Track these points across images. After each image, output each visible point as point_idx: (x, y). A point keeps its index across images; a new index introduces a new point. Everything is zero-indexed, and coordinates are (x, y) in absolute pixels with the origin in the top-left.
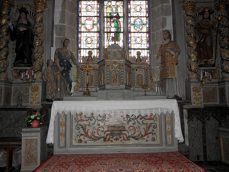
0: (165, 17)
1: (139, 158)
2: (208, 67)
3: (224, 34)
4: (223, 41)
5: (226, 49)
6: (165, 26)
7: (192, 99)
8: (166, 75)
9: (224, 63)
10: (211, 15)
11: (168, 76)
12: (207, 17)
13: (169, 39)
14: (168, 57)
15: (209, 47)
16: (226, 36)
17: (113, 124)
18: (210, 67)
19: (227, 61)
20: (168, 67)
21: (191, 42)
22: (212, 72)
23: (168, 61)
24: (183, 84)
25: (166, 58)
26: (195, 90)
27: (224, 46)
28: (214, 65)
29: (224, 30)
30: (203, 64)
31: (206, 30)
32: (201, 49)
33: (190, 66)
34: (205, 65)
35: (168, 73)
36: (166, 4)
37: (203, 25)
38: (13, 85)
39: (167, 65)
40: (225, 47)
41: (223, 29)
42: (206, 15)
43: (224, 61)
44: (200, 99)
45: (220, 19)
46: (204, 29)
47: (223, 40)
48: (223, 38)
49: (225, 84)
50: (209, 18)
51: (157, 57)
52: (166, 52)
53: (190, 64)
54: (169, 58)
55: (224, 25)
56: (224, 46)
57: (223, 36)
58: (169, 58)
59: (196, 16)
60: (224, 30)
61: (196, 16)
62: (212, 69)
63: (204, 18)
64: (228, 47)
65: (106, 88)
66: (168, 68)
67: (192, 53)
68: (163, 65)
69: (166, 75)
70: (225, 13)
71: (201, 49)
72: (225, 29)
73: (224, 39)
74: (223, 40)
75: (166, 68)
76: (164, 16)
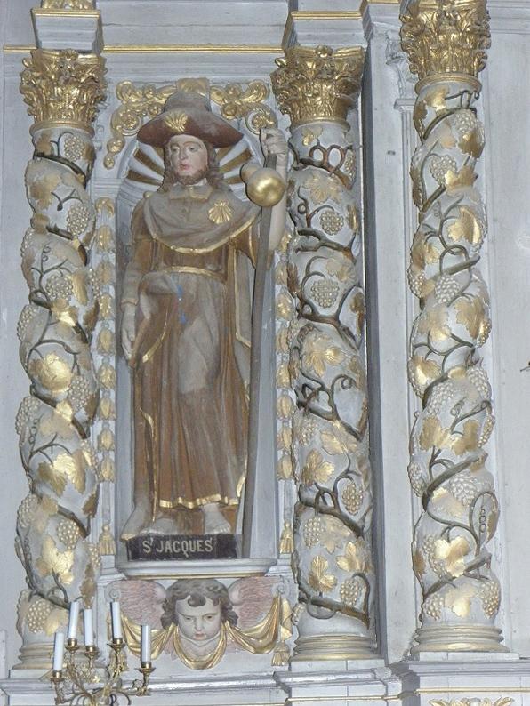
2: (180, 556)
28: (226, 547)
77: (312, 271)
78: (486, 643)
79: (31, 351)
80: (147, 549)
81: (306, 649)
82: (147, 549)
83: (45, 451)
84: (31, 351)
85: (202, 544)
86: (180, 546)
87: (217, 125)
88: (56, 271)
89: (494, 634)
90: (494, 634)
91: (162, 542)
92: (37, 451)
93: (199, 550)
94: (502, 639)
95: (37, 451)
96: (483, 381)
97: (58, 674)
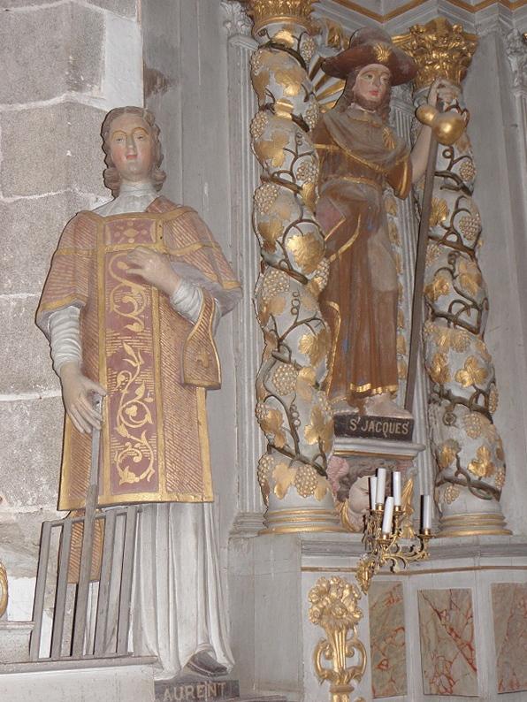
2: (379, 436)
3: (458, 235)
5: (470, 329)
6: (94, 78)
8: (131, 478)
9: (459, 421)
10: (397, 90)
13: (149, 185)
21: (294, 244)
25: (132, 334)
29: (457, 210)
32: (336, 307)
33: (291, 418)
35: (145, 462)
37: (349, 143)
38: (94, 482)
40: (463, 317)
42: (369, 83)
44: (354, 682)
45: (454, 130)
47: (452, 272)
50: (382, 107)
51: (41, 316)
52: (139, 279)
53: (288, 402)
55: (454, 176)
60: (457, 210)
63: (349, 98)
65: (469, 640)
67: (306, 322)
69: (131, 478)
71: (336, 307)
75: (133, 411)
77: (460, 207)
78: (288, 527)
79: (290, 227)
80: (353, 427)
81: (447, 526)
82: (353, 427)
83: (309, 323)
84: (290, 227)
85: (400, 427)
86: (382, 427)
87: (410, 65)
88: (309, 156)
89: (498, 521)
90: (498, 521)
91: (367, 422)
92: (302, 323)
93: (397, 432)
94: (505, 524)
95: (302, 323)
96: (276, 379)
97: (385, 537)
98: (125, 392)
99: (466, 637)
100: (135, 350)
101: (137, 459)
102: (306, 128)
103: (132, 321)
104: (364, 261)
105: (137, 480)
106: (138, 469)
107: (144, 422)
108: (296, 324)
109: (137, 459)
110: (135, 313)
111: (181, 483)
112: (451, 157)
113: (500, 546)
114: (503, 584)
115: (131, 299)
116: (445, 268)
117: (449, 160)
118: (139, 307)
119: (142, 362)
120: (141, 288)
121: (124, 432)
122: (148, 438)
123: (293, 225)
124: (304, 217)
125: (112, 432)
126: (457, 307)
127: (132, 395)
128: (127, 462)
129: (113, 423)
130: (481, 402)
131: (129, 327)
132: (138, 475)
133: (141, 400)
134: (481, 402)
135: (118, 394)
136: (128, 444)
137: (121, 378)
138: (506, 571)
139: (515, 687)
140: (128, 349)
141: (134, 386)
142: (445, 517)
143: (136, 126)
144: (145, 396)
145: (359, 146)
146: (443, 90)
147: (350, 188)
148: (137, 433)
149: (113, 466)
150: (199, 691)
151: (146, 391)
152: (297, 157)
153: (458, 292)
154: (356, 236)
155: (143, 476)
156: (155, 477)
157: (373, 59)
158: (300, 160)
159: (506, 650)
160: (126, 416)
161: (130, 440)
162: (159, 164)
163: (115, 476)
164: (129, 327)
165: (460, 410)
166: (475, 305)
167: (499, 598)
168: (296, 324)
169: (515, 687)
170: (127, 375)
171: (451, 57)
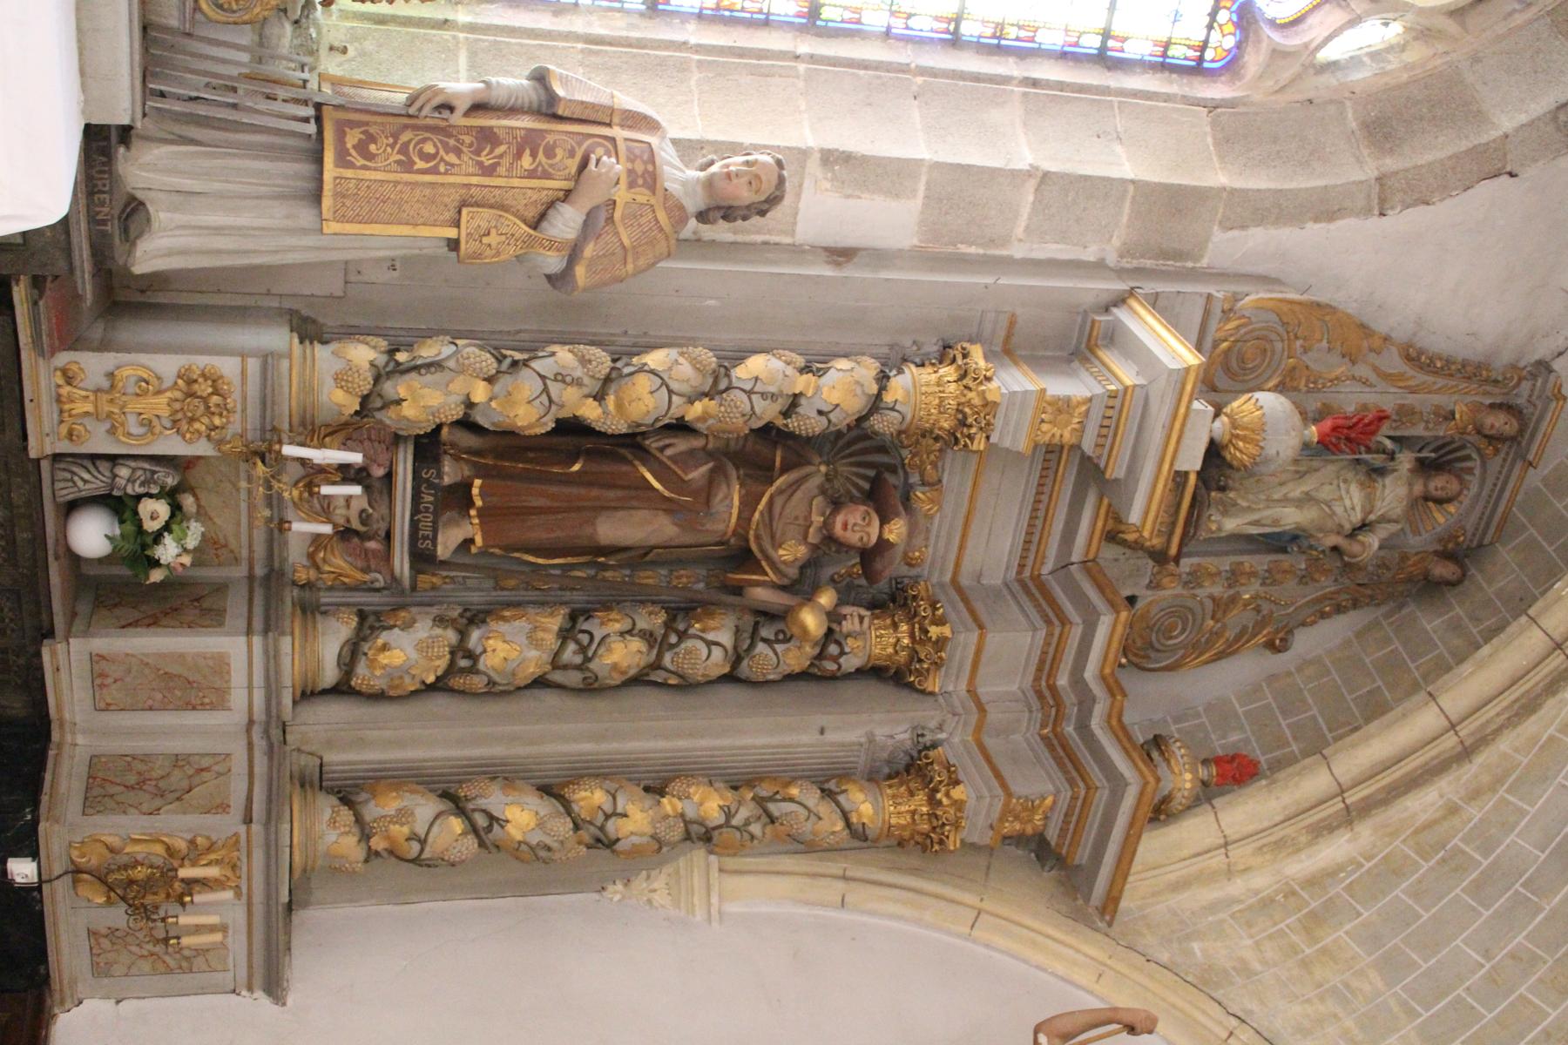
0: (914, 191)
1: (1205, 274)
2: (415, 510)
4: (622, 634)
5: (557, 654)
7: (108, 360)
9: (439, 631)
11: (343, 160)
12: (838, 529)
13: (702, 207)
14: (531, 174)
15: (588, 530)
16: (660, 656)
17: (1058, 775)
18: (414, 526)
19: (452, 653)
20: (434, 171)
22: (363, 537)
23: (489, 171)
24: (268, 293)
25: (519, 155)
26: (192, 395)
27: (577, 642)
30: (440, 475)
31: (735, 512)
32: (576, 467)
34: (431, 485)
35: (370, 157)
36: (1025, 211)
37: (780, 492)
39: (452, 158)
40: (572, 647)
41: (725, 637)
43: (451, 636)
46: (749, 504)
47: (629, 632)
48: (648, 636)
49: (249, 632)
54: (516, 182)
55: (752, 646)
56: (577, 642)
57: (665, 636)
58: (516, 182)
59: (867, 444)
60: (710, 644)
61: (867, 444)
62: (388, 536)
64: (565, 667)
66: (420, 165)
67: (546, 390)
68: (457, 119)
69: (353, 138)
70: (842, 660)
72: (717, 653)
73: (636, 644)
74: (629, 632)
75: (429, 148)
76: (924, 179)
98: (452, 142)
99: (164, 622)
100: (501, 156)
101: (373, 147)
102: (786, 414)
103: (534, 155)
104: (635, 503)
105: (349, 146)
106: (362, 148)
107: (416, 159)
108: (543, 378)
109: (373, 147)
110: (544, 160)
111: (344, 196)
112: (778, 641)
113: (278, 672)
114: (228, 673)
115: (559, 157)
116: (634, 624)
117: (772, 637)
118: (551, 166)
119: (487, 163)
120: (574, 170)
121: (404, 138)
122: (398, 162)
123: (664, 383)
124: (675, 398)
125: (406, 127)
126: (585, 638)
127: (448, 150)
128: (372, 139)
129: (415, 128)
130: (464, 663)
131: (528, 152)
132: (354, 147)
133: (442, 159)
134: (464, 663)
135: (450, 136)
136: (391, 140)
137: (467, 139)
138: (246, 771)
139: (98, 681)
140: (502, 149)
141: (458, 152)
142: (318, 617)
143: (909, 417)
144: (447, 164)
145: (779, 502)
146: (856, 620)
147: (724, 487)
148: (404, 150)
149: (367, 124)
150: (102, 196)
151: (453, 165)
152: (749, 393)
153: (603, 639)
154: (667, 493)
155: (353, 152)
156: (351, 165)
157: (884, 521)
158: (744, 397)
159: (147, 671)
160: (424, 140)
161: (395, 142)
162: (725, 218)
163: (353, 124)
164: (528, 152)
165: (451, 636)
166: (588, 660)
167: (211, 663)
168: (543, 378)
169: (98, 681)
170: (471, 145)
171: (903, 649)
